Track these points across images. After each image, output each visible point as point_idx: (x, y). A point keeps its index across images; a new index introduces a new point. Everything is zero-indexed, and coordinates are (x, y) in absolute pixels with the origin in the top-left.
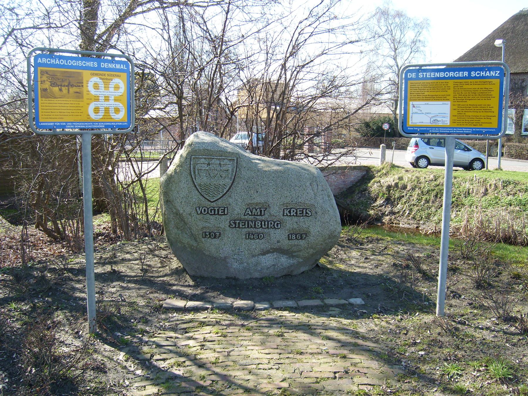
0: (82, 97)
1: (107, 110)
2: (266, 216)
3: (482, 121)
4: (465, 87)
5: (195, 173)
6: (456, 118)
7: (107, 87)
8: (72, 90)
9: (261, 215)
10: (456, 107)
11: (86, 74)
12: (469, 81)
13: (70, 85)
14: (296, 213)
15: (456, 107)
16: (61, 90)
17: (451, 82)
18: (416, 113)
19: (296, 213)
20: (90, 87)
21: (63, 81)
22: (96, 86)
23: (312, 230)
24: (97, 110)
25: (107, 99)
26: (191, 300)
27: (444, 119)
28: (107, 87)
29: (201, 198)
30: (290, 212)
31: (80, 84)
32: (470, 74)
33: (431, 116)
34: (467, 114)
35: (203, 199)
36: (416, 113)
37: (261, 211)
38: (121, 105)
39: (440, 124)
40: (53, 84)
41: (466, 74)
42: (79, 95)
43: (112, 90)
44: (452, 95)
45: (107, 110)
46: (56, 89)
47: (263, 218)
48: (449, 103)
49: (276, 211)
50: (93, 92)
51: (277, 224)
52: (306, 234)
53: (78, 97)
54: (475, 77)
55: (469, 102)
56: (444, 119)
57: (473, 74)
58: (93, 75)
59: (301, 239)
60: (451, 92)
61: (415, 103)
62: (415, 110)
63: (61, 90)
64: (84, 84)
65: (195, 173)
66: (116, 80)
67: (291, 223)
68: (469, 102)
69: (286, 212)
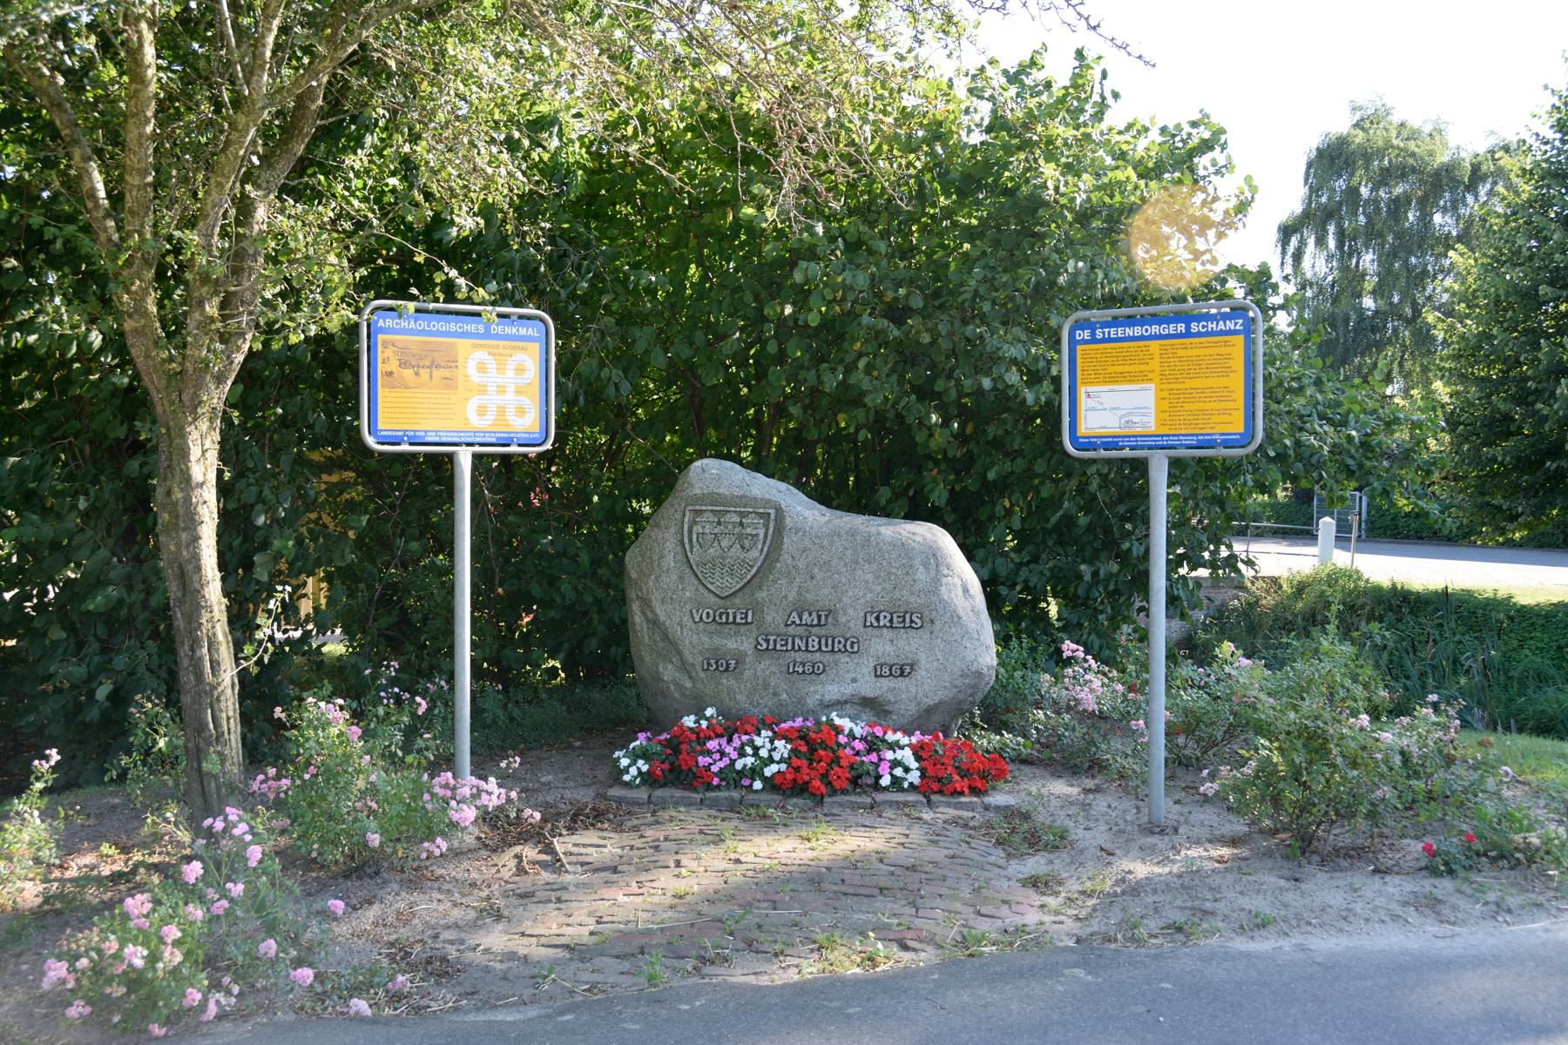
0: (456, 388)
1: (501, 411)
2: (830, 626)
3: (1215, 419)
4: (1181, 353)
5: (690, 540)
6: (1166, 416)
7: (501, 369)
8: (437, 374)
9: (819, 625)
10: (1165, 394)
11: (463, 344)
12: (1188, 341)
13: (434, 365)
14: (891, 621)
15: (1165, 394)
16: (417, 374)
17: (1155, 345)
18: (1093, 409)
19: (891, 621)
20: (471, 369)
21: (421, 358)
22: (482, 368)
23: (922, 657)
24: (482, 410)
25: (501, 390)
26: (803, 990)
27: (1145, 419)
28: (501, 369)
29: (701, 588)
30: (877, 619)
31: (452, 363)
32: (1188, 328)
33: (1120, 413)
34: (1187, 407)
35: (706, 594)
36: (1093, 409)
37: (819, 617)
38: (528, 401)
39: (1138, 430)
40: (403, 364)
41: (1181, 327)
42: (450, 383)
43: (510, 373)
44: (1158, 369)
45: (501, 411)
46: (409, 372)
47: (822, 631)
48: (1152, 386)
49: (851, 619)
50: (475, 376)
51: (851, 647)
52: (912, 666)
53: (449, 387)
54: (1199, 335)
55: (1190, 384)
56: (1145, 419)
57: (1194, 327)
58: (476, 346)
59: (902, 674)
60: (1155, 365)
61: (1090, 389)
62: (1091, 403)
63: (417, 374)
64: (460, 364)
65: (690, 540)
66: (520, 356)
67: (883, 646)
68: (1190, 384)
69: (871, 619)
